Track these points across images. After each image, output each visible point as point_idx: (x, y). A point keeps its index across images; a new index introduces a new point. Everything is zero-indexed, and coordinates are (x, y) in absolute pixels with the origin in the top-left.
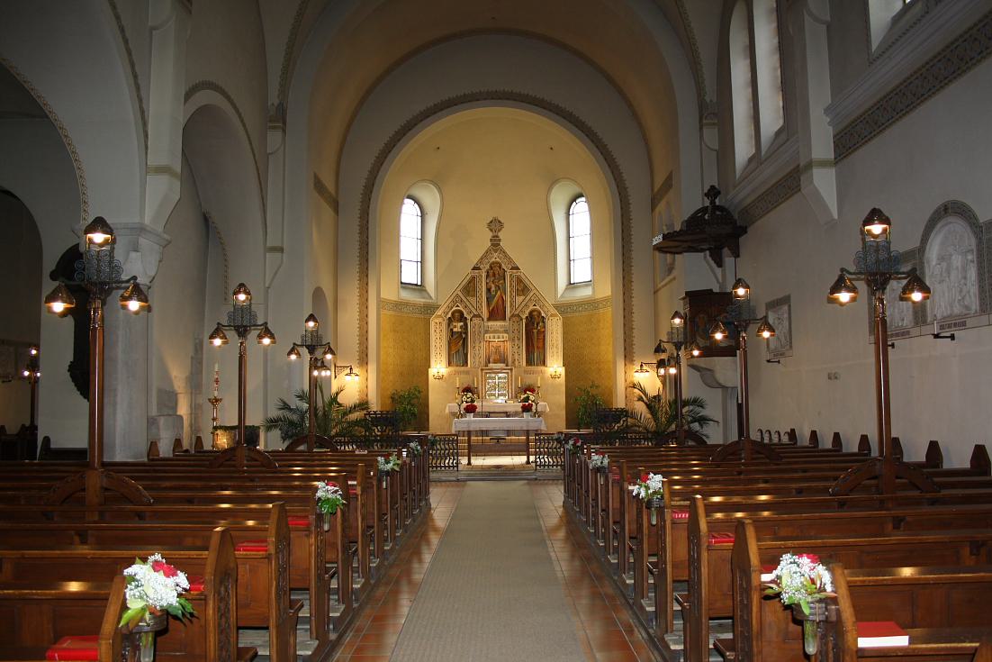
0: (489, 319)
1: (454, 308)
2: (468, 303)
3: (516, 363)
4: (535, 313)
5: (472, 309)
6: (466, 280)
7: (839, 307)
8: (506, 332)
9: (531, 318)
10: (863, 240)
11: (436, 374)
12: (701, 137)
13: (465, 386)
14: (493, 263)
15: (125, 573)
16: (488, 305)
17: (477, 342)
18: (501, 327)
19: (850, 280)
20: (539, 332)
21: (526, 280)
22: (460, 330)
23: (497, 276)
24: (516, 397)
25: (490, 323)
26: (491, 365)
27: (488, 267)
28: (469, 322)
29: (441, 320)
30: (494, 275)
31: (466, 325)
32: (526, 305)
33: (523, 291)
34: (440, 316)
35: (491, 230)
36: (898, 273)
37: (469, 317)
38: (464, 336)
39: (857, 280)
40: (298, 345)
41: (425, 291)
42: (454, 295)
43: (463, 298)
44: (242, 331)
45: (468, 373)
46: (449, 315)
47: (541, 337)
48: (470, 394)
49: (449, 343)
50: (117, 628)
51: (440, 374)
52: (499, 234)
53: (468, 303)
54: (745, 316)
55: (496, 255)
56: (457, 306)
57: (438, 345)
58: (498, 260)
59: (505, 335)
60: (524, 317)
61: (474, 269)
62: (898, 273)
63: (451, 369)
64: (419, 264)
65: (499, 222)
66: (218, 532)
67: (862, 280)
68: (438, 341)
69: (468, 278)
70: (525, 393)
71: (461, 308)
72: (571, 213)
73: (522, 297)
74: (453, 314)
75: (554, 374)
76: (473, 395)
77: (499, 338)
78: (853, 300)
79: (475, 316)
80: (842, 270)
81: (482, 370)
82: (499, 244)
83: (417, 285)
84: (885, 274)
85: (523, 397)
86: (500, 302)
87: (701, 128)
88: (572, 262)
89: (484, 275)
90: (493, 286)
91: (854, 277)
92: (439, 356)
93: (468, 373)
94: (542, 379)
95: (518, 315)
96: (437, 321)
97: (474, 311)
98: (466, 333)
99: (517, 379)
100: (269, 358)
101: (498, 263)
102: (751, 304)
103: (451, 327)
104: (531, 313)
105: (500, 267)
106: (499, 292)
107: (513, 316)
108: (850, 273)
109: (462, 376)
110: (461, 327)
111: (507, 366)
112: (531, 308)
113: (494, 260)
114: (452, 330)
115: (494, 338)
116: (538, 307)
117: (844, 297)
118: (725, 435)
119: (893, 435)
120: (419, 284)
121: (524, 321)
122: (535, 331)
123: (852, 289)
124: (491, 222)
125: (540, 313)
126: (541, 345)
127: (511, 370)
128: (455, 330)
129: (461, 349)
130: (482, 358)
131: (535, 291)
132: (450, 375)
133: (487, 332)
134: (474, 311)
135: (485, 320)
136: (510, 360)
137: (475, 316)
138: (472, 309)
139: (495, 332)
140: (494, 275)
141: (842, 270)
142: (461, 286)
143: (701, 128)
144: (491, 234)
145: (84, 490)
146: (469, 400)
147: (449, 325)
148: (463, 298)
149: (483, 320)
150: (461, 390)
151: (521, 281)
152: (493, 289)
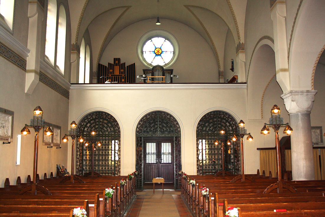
7: (264, 135)
10: (272, 115)
12: (198, 144)
19: (268, 127)
36: (283, 125)
39: (270, 127)
40: (28, 126)
44: (37, 129)
54: (243, 133)
62: (283, 125)
66: (86, 201)
67: (271, 127)
78: (269, 133)
80: (265, 124)
84: (278, 125)
87: (219, 78)
91: (268, 126)
102: (245, 129)
108: (268, 125)
117: (265, 132)
118: (318, 178)
119: (38, 173)
123: (268, 130)
141: (265, 124)
143: (219, 78)
145: (31, 190)
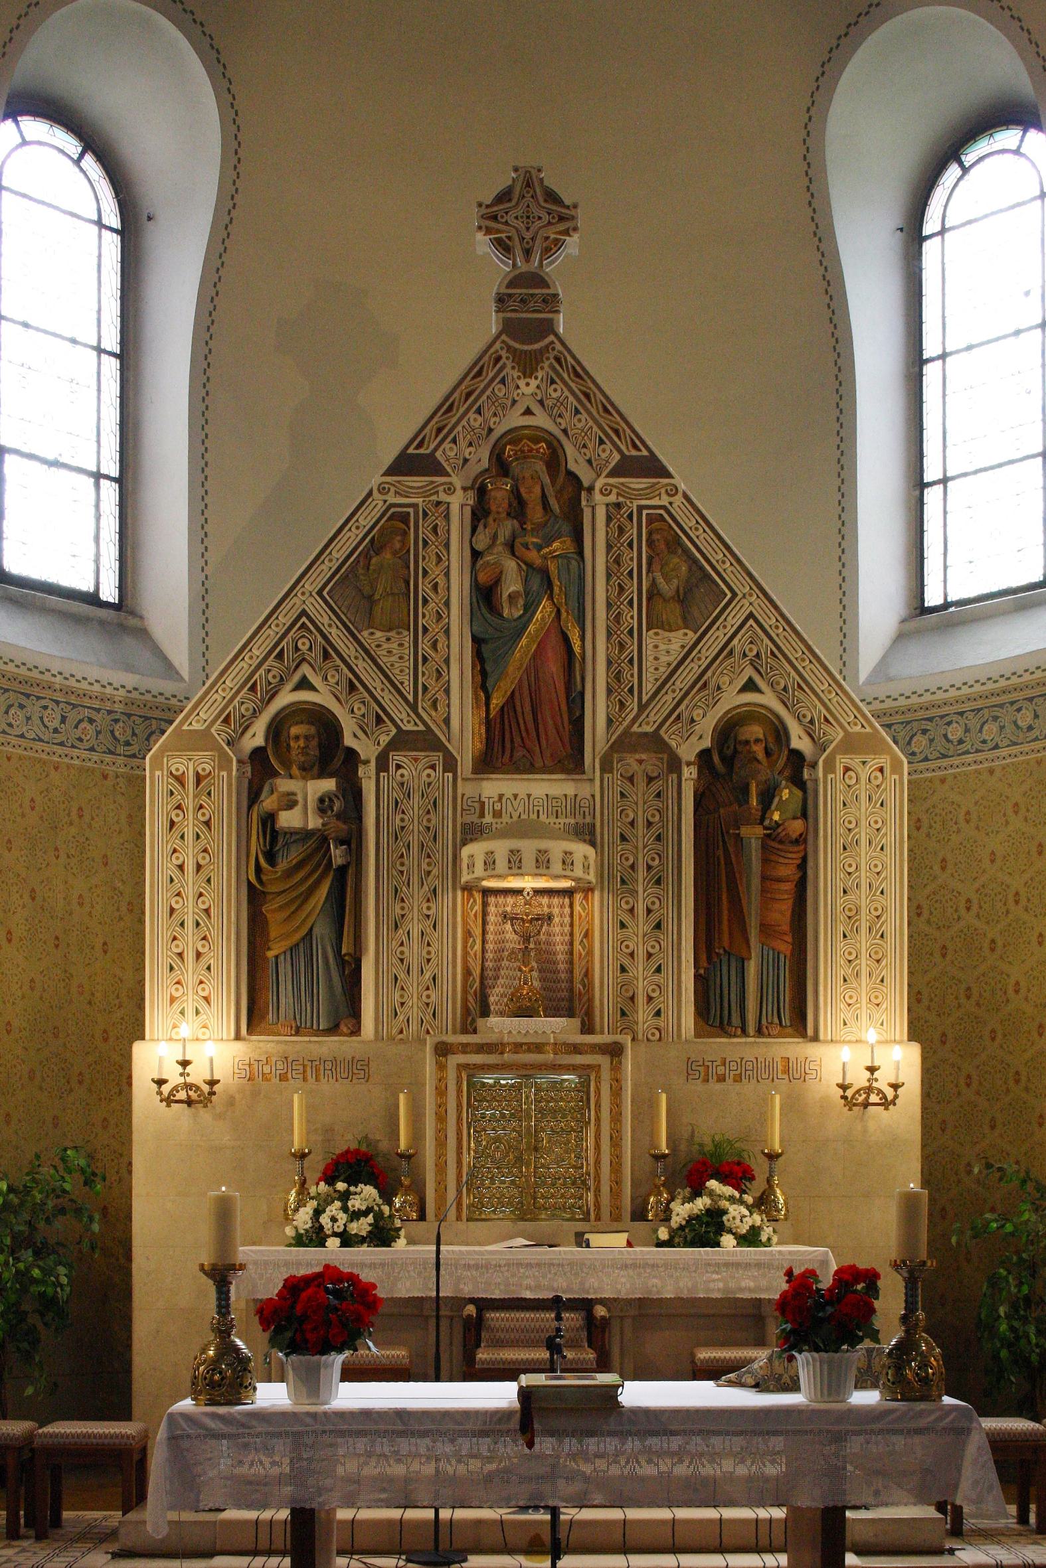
0: (486, 764)
1: (286, 698)
2: (363, 667)
3: (643, 1015)
4: (755, 731)
5: (388, 698)
6: (351, 537)
8: (586, 833)
9: (729, 761)
11: (174, 1076)
13: (346, 1142)
14: (513, 436)
15: (708, 1184)
16: (483, 682)
17: (416, 895)
18: (555, 806)
20: (773, 838)
21: (703, 538)
22: (314, 822)
23: (536, 514)
24: (639, 1214)
25: (494, 787)
26: (499, 1026)
27: (481, 457)
28: (367, 777)
29: (204, 762)
30: (518, 508)
31: (352, 793)
32: (700, 683)
33: (683, 598)
34: (201, 740)
35: (503, 246)
37: (367, 749)
38: (338, 855)
41: (143, 634)
42: (285, 619)
43: (336, 634)
45: (357, 1069)
46: (256, 737)
47: (787, 869)
48: (366, 1195)
49: (255, 896)
50: (584, 1233)
51: (198, 1074)
52: (550, 269)
53: (363, 667)
55: (529, 387)
56: (304, 684)
57: (189, 911)
58: (541, 420)
59: (581, 850)
60: (688, 751)
61: (405, 465)
63: (264, 1045)
64: (110, 492)
65: (552, 197)
68: (190, 883)
69: (365, 520)
70: (697, 1192)
71: (322, 697)
72: (930, 226)
73: (678, 640)
74: (276, 730)
75: (860, 1079)
76: (387, 1197)
77: (542, 863)
79: (402, 741)
81: (443, 1050)
82: (547, 328)
83: (92, 599)
85: (681, 1211)
86: (553, 667)
88: (932, 496)
89: (459, 502)
90: (511, 566)
92: (190, 972)
93: (357, 1069)
94: (793, 1106)
95: (655, 742)
96: (179, 765)
97: (401, 713)
98: (353, 841)
99: (645, 1110)
100: (692, 1311)
101: (538, 435)
103: (268, 802)
104: (727, 731)
105: (554, 460)
106: (543, 611)
107: (624, 744)
109: (327, 1086)
110: (324, 805)
111: (588, 1028)
112: (732, 699)
113: (515, 419)
114: (269, 819)
115: (515, 864)
116: (768, 699)
120: (109, 593)
121: (689, 773)
122: (752, 834)
124: (504, 197)
125: (780, 733)
126: (782, 913)
127: (615, 1051)
128: (288, 820)
129: (323, 930)
130: (446, 986)
131: (754, 604)
132: (253, 1075)
133: (471, 833)
134: (401, 713)
135: (466, 762)
136: (605, 999)
137: (402, 741)
138: (388, 698)
139: (523, 829)
140: (518, 508)
142: (326, 568)
144: (500, 268)
146: (362, 1227)
147: (254, 797)
148: (336, 634)
149: (450, 764)
150: (317, 1164)
151: (674, 544)
152: (512, 584)
